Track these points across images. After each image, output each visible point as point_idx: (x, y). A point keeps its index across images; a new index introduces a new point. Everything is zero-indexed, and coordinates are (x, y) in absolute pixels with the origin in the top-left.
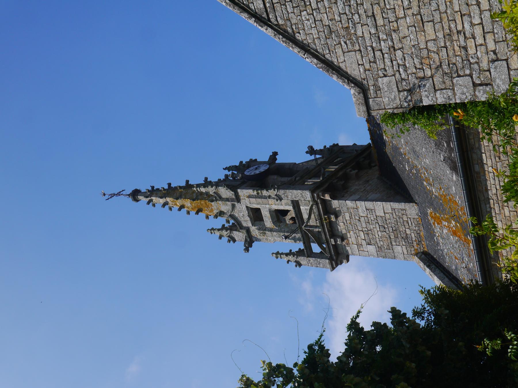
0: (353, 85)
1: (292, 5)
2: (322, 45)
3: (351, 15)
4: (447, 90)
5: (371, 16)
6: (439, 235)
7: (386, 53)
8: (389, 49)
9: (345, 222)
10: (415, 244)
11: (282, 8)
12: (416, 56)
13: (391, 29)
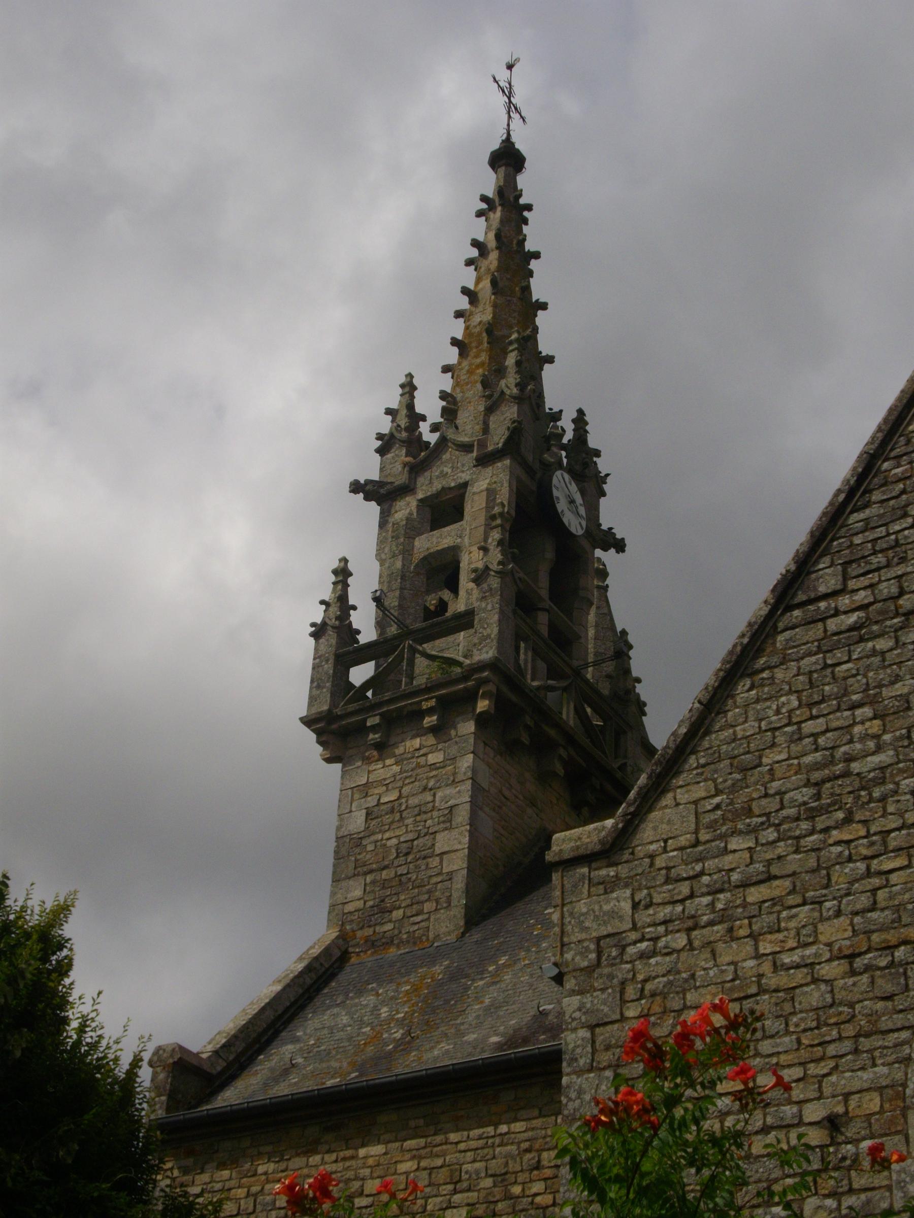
0: (620, 826)
1: (815, 671)
2: (719, 746)
3: (777, 822)
4: (590, 1056)
5: (768, 871)
6: (381, 995)
7: (684, 910)
8: (693, 917)
9: (422, 752)
10: (368, 932)
11: (812, 642)
12: (670, 983)
13: (735, 921)
